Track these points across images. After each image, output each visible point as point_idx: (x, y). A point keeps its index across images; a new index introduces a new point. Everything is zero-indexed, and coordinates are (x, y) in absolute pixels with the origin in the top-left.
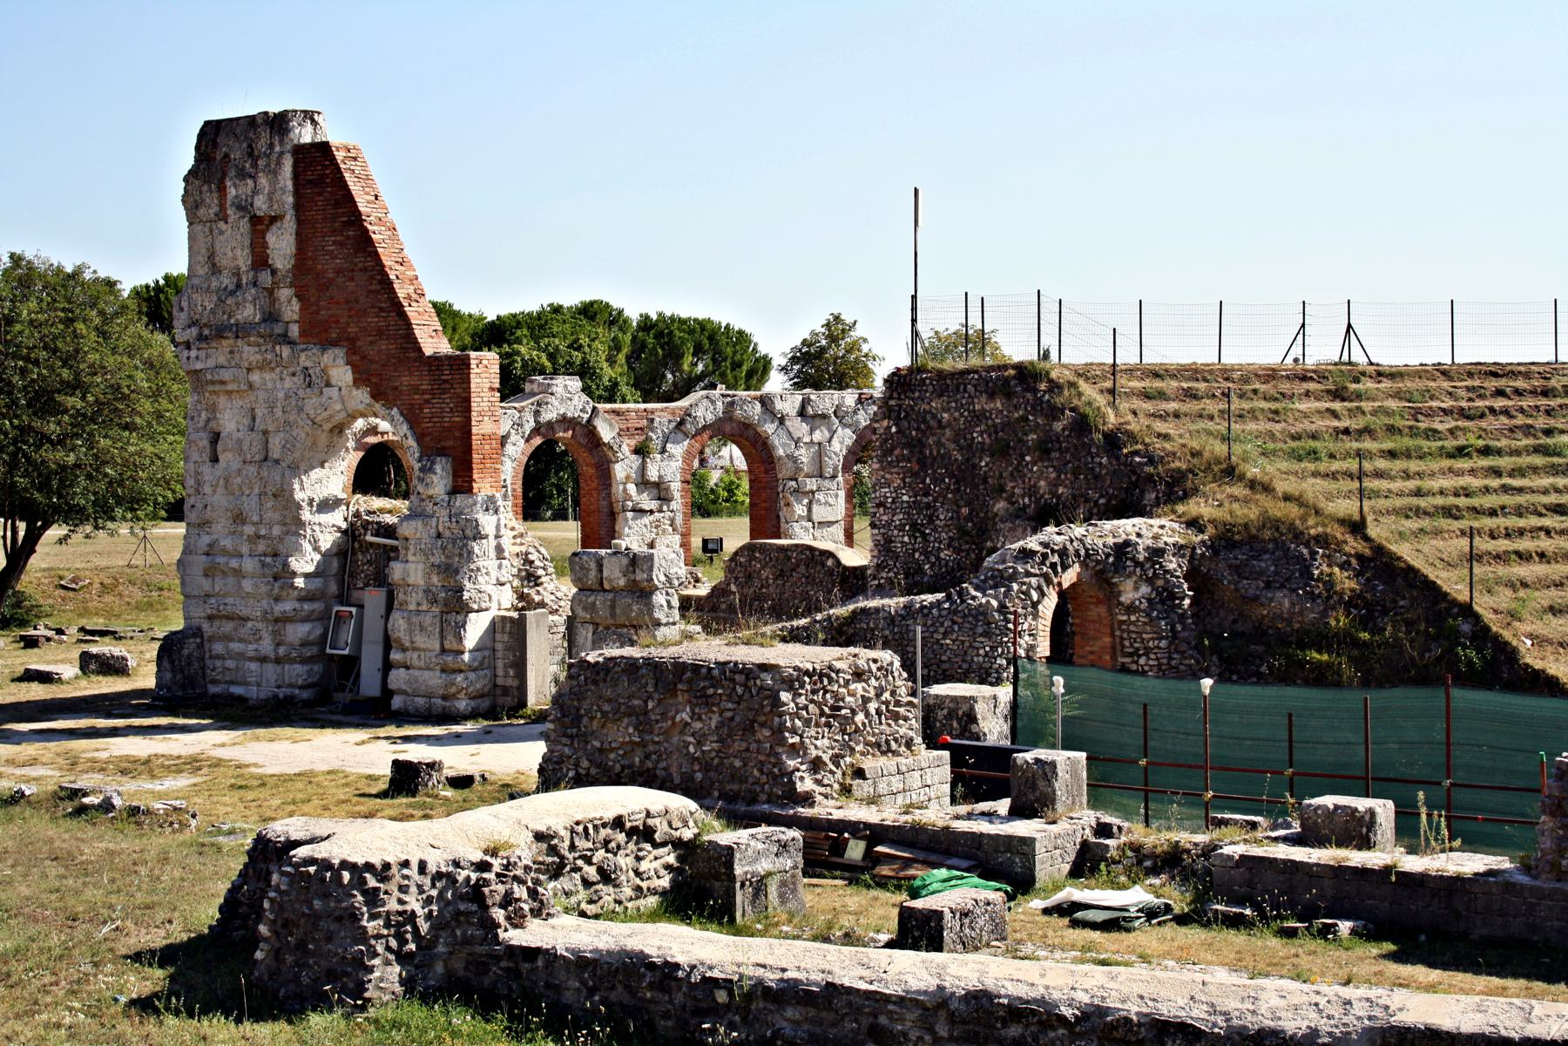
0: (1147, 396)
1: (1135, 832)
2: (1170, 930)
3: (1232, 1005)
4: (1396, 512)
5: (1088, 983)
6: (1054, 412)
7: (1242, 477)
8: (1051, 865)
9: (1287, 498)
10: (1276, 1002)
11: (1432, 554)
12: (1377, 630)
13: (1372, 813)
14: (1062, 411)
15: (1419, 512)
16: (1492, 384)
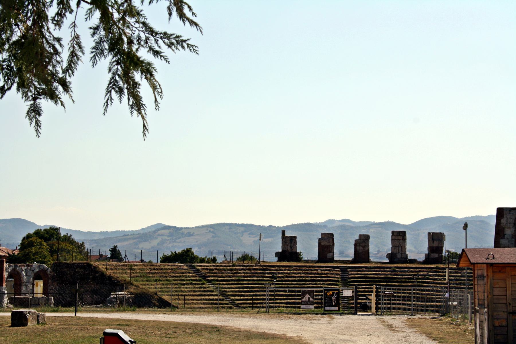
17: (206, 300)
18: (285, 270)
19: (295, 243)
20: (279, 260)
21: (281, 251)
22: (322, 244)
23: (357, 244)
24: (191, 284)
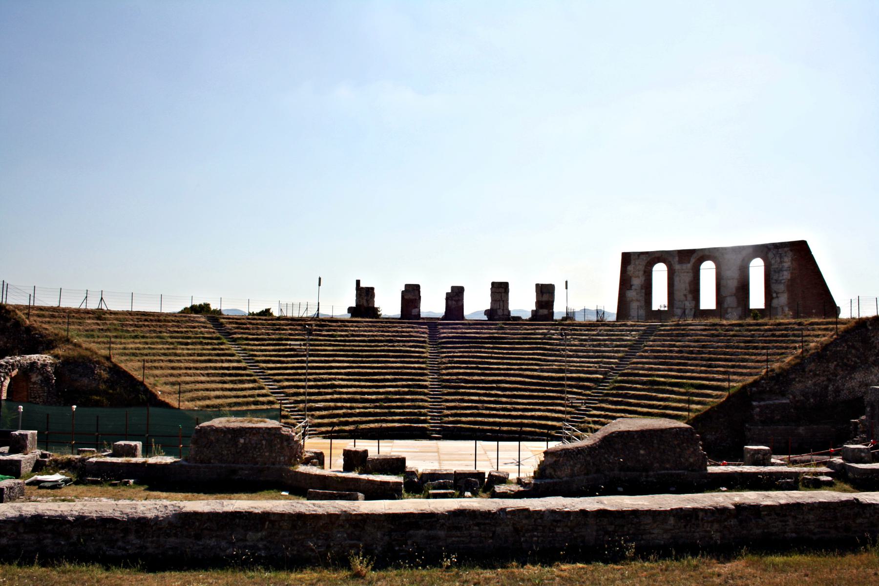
0: (38, 316)
1: (54, 455)
2: (73, 487)
3: (128, 511)
4: (118, 354)
5: (77, 508)
6: (8, 320)
7: (72, 342)
8: (26, 468)
9: (86, 349)
10: (142, 508)
11: (132, 367)
12: (115, 389)
13: (136, 446)
14: (10, 319)
15: (126, 355)
16: (144, 317)
17: (215, 368)
18: (352, 326)
19: (373, 295)
20: (352, 316)
21: (354, 305)
22: (406, 297)
23: (449, 297)
24: (201, 343)
